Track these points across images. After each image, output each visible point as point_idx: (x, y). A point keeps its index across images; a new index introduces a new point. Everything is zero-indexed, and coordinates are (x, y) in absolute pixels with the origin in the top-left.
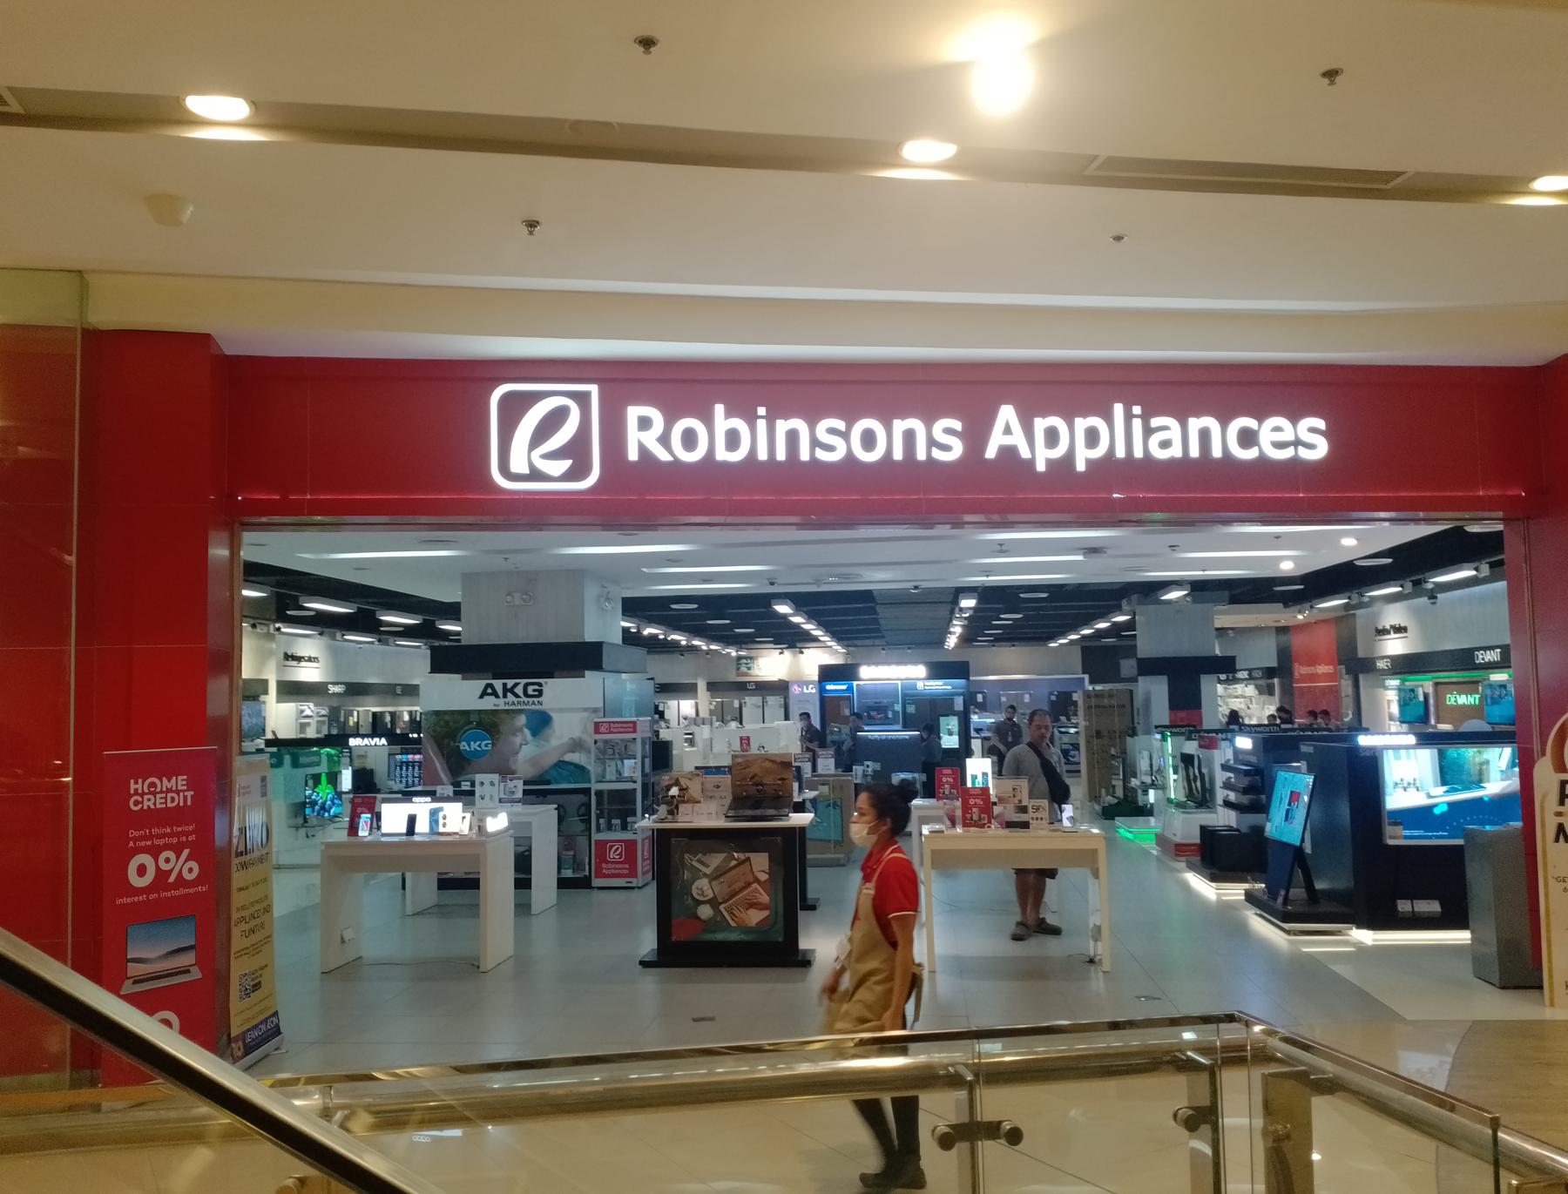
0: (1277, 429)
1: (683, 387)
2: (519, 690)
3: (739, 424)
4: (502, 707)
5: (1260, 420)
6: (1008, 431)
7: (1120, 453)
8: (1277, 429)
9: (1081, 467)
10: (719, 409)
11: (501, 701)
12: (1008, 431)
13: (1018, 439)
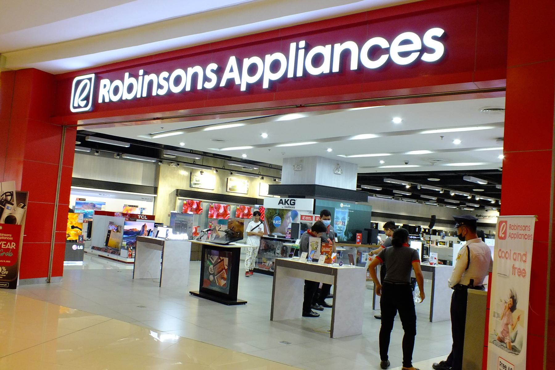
0: (406, 42)
1: (113, 70)
2: (289, 202)
3: (133, 80)
4: (284, 208)
5: (390, 40)
6: (231, 70)
7: (290, 75)
8: (406, 42)
9: (266, 85)
10: (127, 74)
11: (284, 206)
12: (231, 70)
13: (235, 75)
